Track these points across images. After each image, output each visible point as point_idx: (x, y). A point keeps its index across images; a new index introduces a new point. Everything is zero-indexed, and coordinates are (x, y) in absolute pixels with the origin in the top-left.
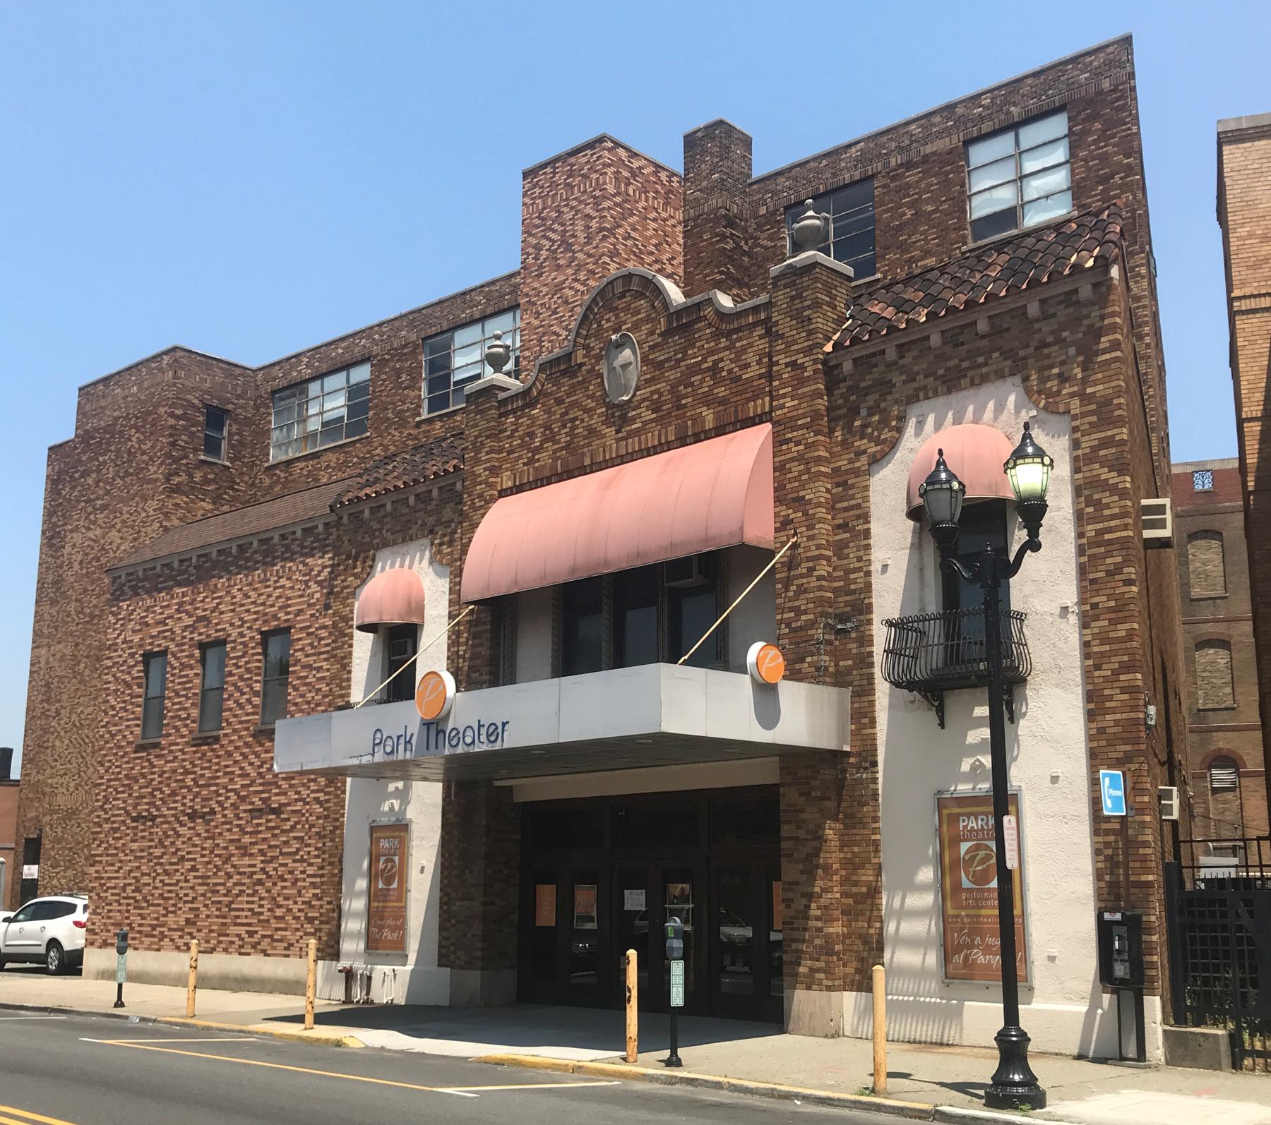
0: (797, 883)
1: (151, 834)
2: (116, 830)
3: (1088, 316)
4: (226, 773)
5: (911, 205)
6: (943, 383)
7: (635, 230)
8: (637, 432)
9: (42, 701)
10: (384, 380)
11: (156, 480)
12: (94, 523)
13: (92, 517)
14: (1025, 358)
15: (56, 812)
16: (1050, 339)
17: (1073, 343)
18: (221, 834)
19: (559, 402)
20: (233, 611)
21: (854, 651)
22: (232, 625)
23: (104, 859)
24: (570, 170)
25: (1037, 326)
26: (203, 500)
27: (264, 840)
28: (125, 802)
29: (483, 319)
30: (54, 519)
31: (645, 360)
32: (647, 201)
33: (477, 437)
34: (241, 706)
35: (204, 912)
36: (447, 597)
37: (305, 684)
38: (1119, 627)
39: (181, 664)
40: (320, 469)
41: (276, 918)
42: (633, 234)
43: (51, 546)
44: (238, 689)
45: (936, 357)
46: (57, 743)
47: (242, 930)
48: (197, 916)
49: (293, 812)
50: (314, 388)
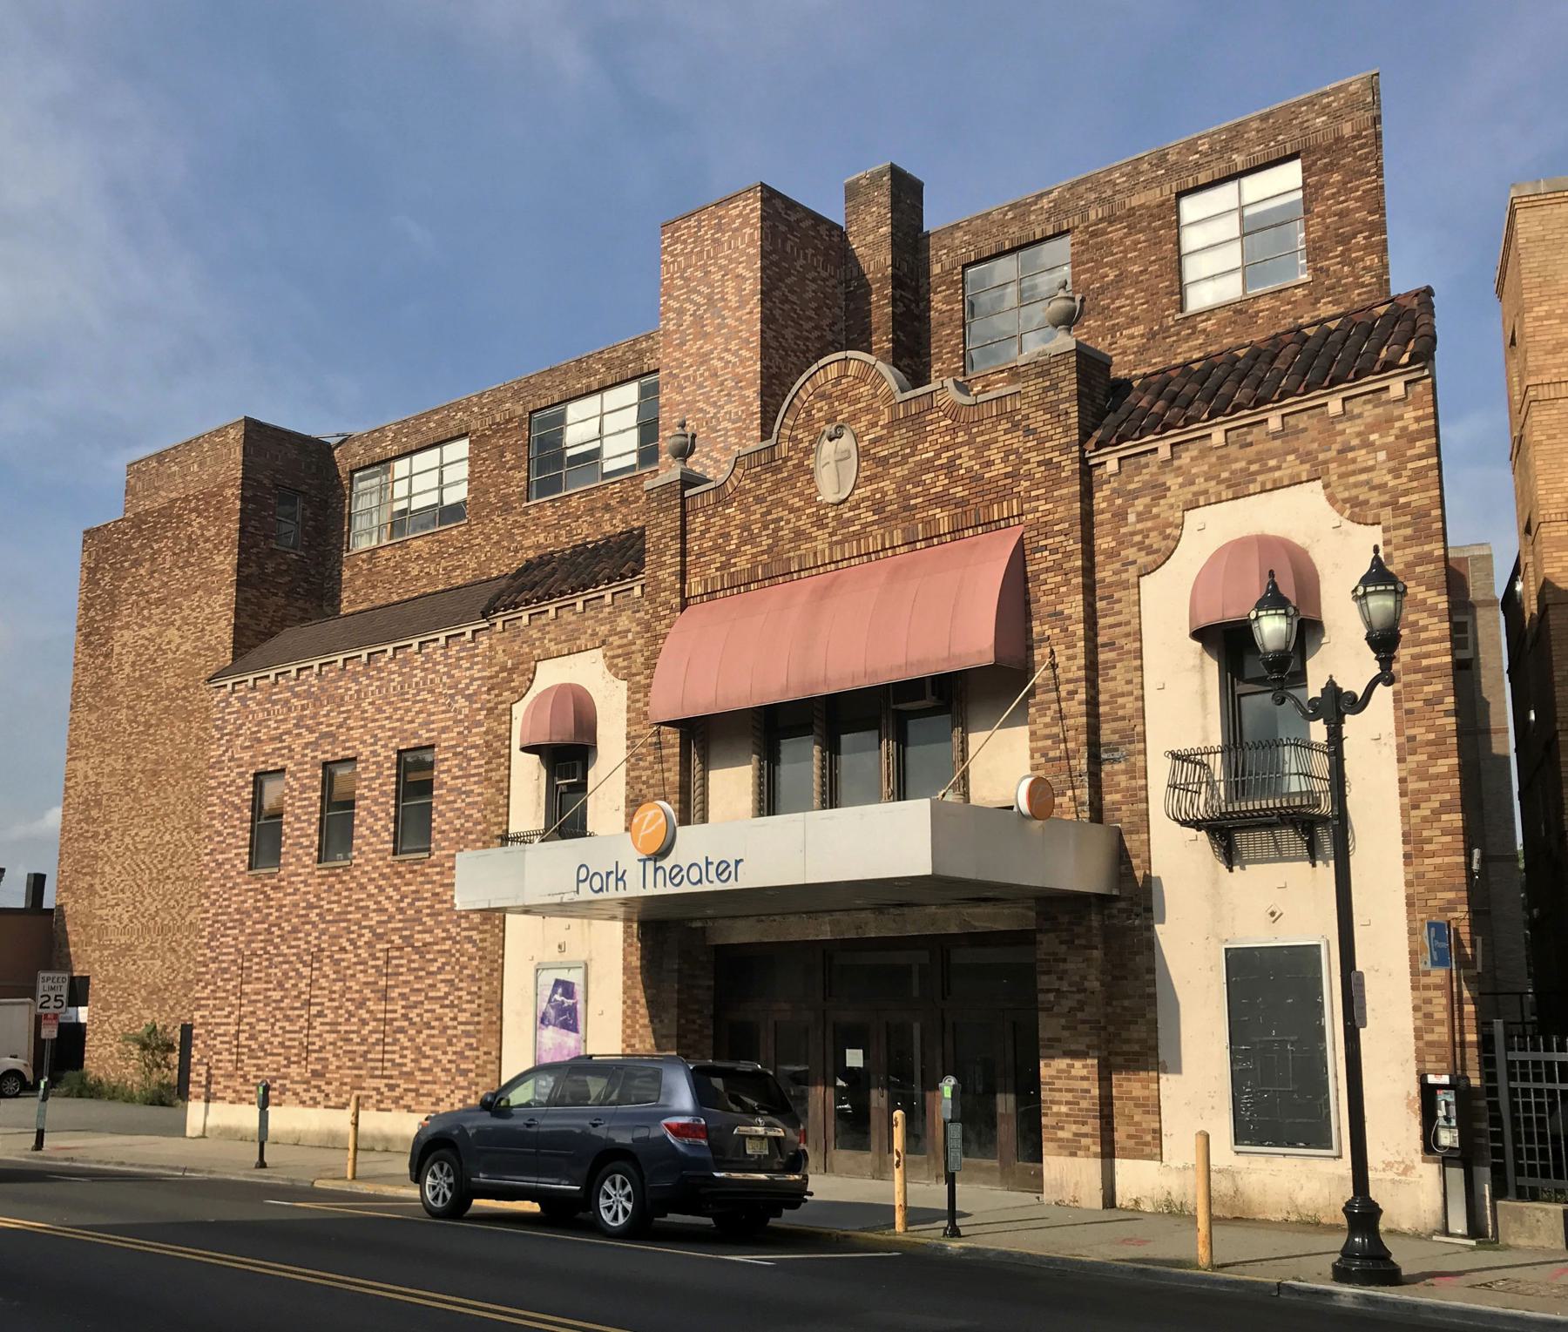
0: (1058, 1040)
1: (268, 975)
2: (225, 970)
3: (1401, 418)
4: (358, 908)
5: (1110, 265)
6: (1228, 487)
7: (792, 292)
8: (857, 536)
9: (79, 822)
10: (485, 460)
11: (222, 572)
12: (149, 619)
13: (146, 612)
14: (1325, 462)
15: (106, 947)
16: (1355, 442)
17: (1382, 448)
18: (353, 976)
19: (759, 500)
20: (364, 726)
21: (1123, 785)
22: (363, 742)
23: (211, 1002)
24: (719, 224)
25: (1339, 427)
26: (276, 595)
27: (406, 982)
28: (235, 939)
29: (602, 389)
30: (92, 613)
31: (863, 454)
32: (805, 258)
33: (660, 538)
34: (375, 833)
35: (334, 1063)
36: (624, 715)
37: (452, 810)
38: (1440, 762)
39: (302, 785)
40: (410, 560)
41: (423, 1070)
42: (793, 298)
43: (88, 644)
44: (372, 814)
45: (1219, 458)
46: (107, 869)
47: (381, 1083)
48: (325, 1067)
49: (439, 951)
50: (401, 467)
